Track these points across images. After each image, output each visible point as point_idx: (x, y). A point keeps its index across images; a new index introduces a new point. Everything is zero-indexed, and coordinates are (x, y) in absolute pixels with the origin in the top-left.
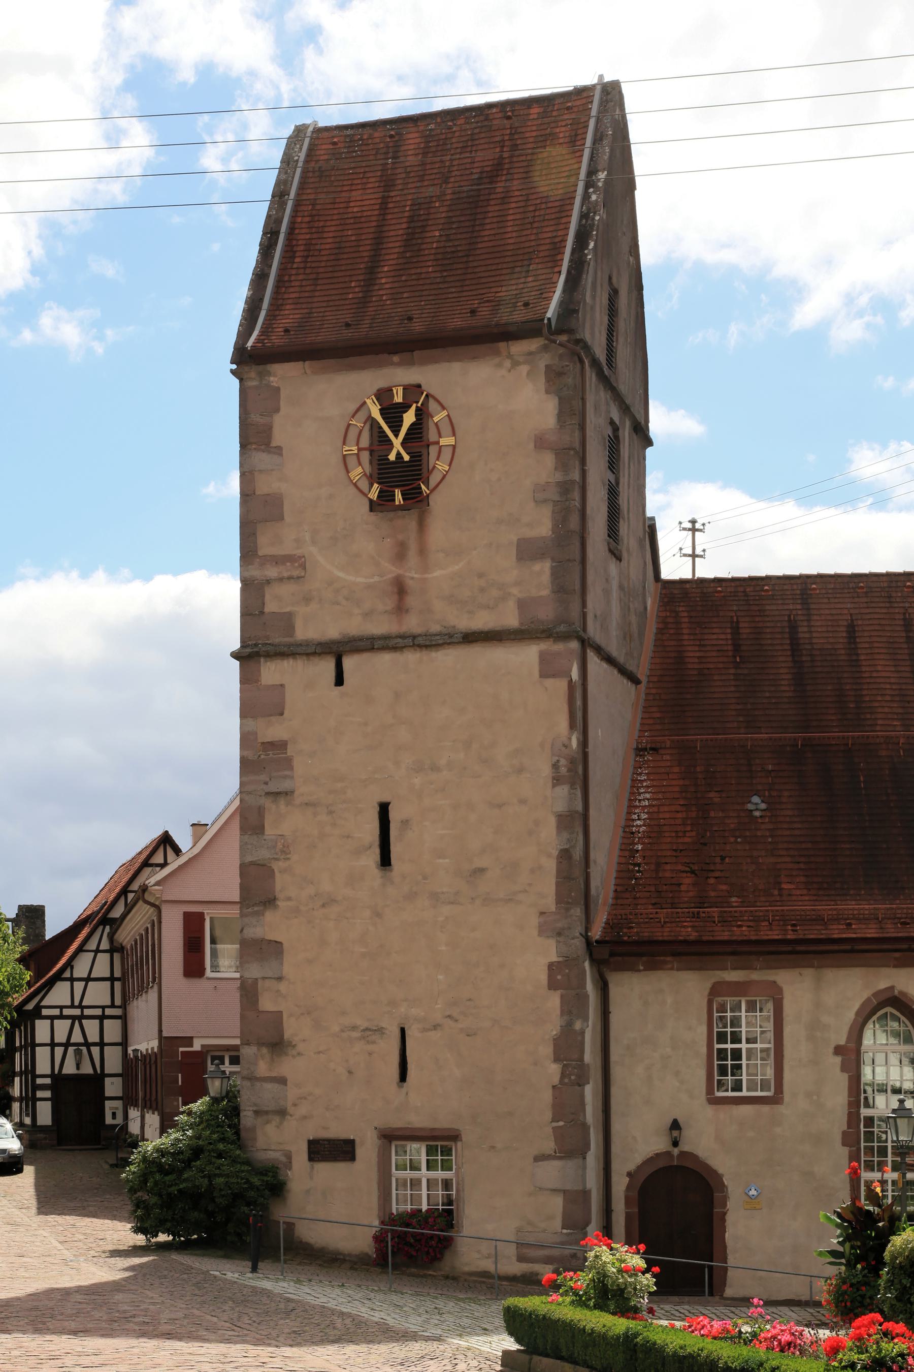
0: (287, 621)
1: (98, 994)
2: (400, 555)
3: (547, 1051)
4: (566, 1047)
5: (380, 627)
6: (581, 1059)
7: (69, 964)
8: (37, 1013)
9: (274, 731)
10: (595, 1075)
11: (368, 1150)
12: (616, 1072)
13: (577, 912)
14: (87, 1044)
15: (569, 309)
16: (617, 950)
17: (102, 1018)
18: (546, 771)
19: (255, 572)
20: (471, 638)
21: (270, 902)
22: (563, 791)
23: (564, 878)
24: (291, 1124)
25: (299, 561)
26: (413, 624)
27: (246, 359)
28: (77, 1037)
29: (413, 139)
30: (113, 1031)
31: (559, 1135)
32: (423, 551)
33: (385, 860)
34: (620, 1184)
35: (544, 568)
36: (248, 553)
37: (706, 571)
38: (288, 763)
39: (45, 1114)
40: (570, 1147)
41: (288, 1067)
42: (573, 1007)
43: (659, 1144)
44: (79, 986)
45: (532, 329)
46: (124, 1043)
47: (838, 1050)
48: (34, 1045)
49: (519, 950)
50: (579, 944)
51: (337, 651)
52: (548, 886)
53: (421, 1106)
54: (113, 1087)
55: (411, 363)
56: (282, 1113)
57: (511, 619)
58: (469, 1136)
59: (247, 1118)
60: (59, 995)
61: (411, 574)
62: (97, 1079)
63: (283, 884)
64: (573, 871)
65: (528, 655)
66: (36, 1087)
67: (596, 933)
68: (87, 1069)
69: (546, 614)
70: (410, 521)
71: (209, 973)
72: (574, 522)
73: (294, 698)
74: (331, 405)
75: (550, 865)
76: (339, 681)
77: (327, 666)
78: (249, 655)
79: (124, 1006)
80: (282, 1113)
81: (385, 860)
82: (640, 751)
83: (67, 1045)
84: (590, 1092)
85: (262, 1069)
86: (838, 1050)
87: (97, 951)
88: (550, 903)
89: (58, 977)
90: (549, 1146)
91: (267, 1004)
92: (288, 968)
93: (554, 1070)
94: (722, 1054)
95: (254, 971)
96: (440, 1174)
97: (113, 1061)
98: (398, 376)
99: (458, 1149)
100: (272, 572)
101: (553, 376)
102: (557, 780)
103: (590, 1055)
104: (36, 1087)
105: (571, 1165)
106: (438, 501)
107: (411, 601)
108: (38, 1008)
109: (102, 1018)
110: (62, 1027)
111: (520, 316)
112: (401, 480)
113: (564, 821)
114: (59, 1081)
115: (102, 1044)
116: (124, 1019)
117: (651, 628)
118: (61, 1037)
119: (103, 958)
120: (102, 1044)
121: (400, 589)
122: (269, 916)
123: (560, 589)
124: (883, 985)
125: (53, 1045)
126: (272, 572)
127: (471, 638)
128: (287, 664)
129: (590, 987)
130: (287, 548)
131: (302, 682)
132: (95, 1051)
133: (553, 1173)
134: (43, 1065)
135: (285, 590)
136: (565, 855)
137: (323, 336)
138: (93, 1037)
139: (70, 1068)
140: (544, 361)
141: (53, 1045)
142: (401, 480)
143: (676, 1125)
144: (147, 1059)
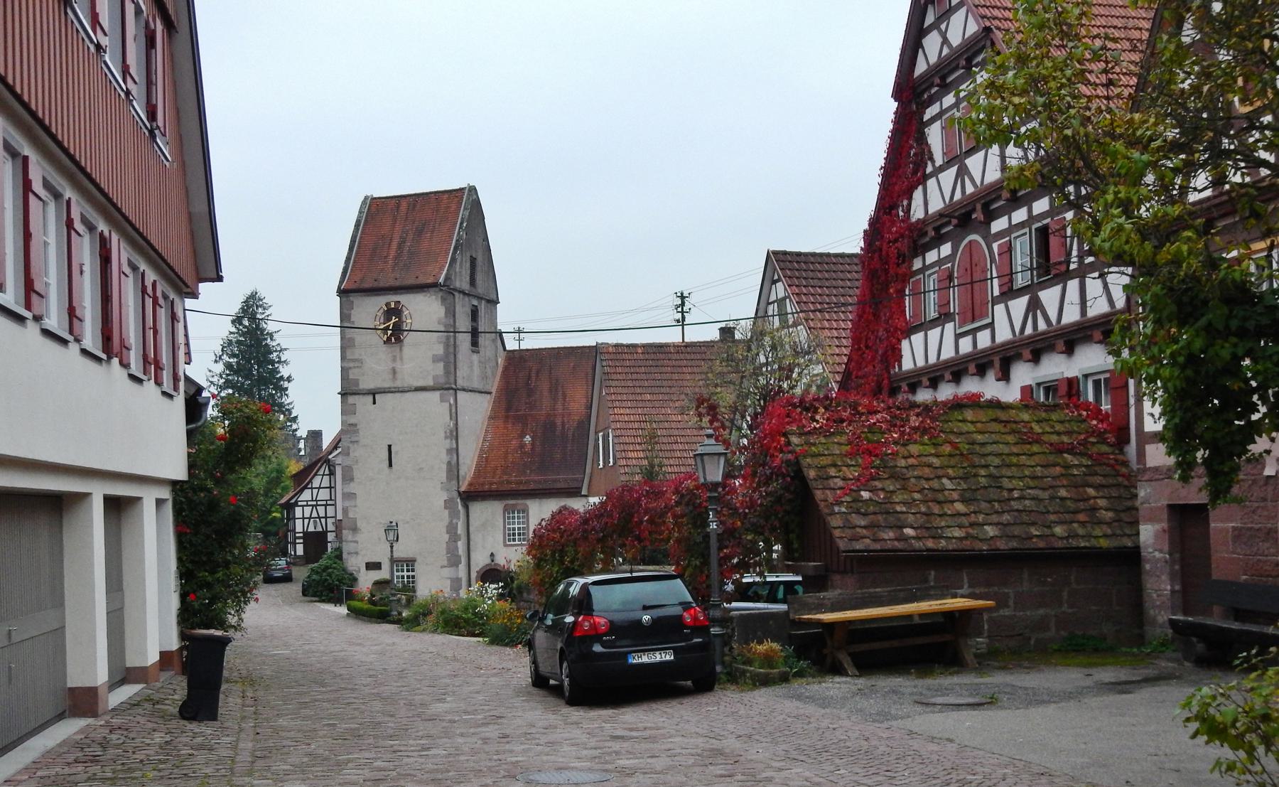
0: (356, 382)
2: (394, 360)
3: (444, 530)
4: (451, 529)
5: (386, 385)
6: (1215, 219)
7: (311, 481)
8: (296, 504)
9: (352, 420)
10: (464, 539)
12: (472, 536)
13: (454, 482)
15: (447, 278)
16: (470, 497)
17: (326, 505)
18: (443, 435)
19: (346, 365)
20: (418, 389)
21: (352, 479)
22: (448, 441)
23: (449, 471)
24: (360, 557)
25: (360, 361)
26: (398, 384)
27: (342, 292)
28: (315, 514)
29: (404, 204)
31: (449, 560)
32: (401, 359)
33: (390, 465)
34: (474, 575)
35: (441, 365)
36: (343, 358)
38: (357, 431)
39: (300, 550)
40: (454, 562)
41: (359, 537)
42: (454, 514)
43: (488, 561)
44: (315, 491)
45: (435, 285)
48: (295, 519)
49: (432, 496)
50: (455, 494)
51: (373, 393)
52: (444, 475)
53: (401, 551)
56: (357, 553)
57: (430, 383)
58: (419, 560)
59: (345, 556)
60: (306, 495)
61: (398, 365)
62: (324, 534)
63: (356, 474)
64: (453, 470)
65: (437, 394)
66: (296, 538)
67: (462, 489)
69: (442, 380)
70: (397, 348)
72: (451, 350)
74: (370, 310)
75: (444, 467)
77: (370, 398)
78: (344, 394)
80: (357, 553)
81: (390, 465)
83: (310, 518)
84: (461, 545)
85: (350, 538)
88: (444, 479)
89: (306, 487)
90: (445, 563)
91: (351, 515)
92: (359, 501)
93: (446, 537)
95: (347, 504)
98: (392, 299)
99: (417, 566)
100: (351, 365)
101: (443, 300)
102: (446, 438)
103: (461, 530)
104: (296, 538)
105: (452, 569)
107: (399, 376)
108: (297, 502)
109: (326, 505)
110: (308, 510)
111: (430, 280)
112: (395, 334)
113: (449, 451)
114: (307, 536)
115: (326, 517)
117: (500, 370)
118: (307, 515)
119: (326, 478)
120: (326, 517)
121: (394, 372)
122: (352, 485)
123: (447, 373)
124: (563, 504)
125: (303, 518)
126: (351, 365)
127: (418, 389)
128: (357, 397)
129: (460, 507)
130: (356, 356)
131: (363, 403)
133: (448, 572)
134: (299, 528)
135: (356, 371)
136: (449, 463)
137: (366, 285)
138: (322, 514)
139: (311, 529)
140: (440, 294)
141: (303, 518)
143: (492, 555)
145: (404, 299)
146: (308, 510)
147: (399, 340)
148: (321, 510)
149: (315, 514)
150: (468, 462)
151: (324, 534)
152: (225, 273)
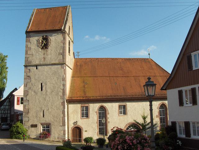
1: (7, 107)
2: (44, 54)
12: (69, 115)
14: (6, 113)
17: (7, 110)
26: (46, 62)
30: (9, 112)
34: (70, 129)
37: (80, 57)
46: (10, 113)
47: (96, 112)
51: (36, 66)
54: (9, 119)
55: (46, 33)
57: (57, 62)
62: (7, 118)
68: (5, 116)
71: (20, 104)
73: (32, 70)
74: (35, 40)
76: (37, 69)
79: (10, 109)
82: (72, 77)
83: (3, 113)
86: (96, 112)
87: (7, 102)
94: (120, 111)
96: (48, 129)
97: (9, 115)
98: (45, 35)
109: (7, 110)
112: (45, 46)
116: (10, 110)
118: (2, 113)
120: (7, 113)
130: (31, 53)
132: (7, 114)
135: (31, 58)
139: (3, 116)
144: (13, 115)
148: (6, 111)
149: (4, 112)
150: (3, 141)
151: (7, 118)
152: (63, 5)
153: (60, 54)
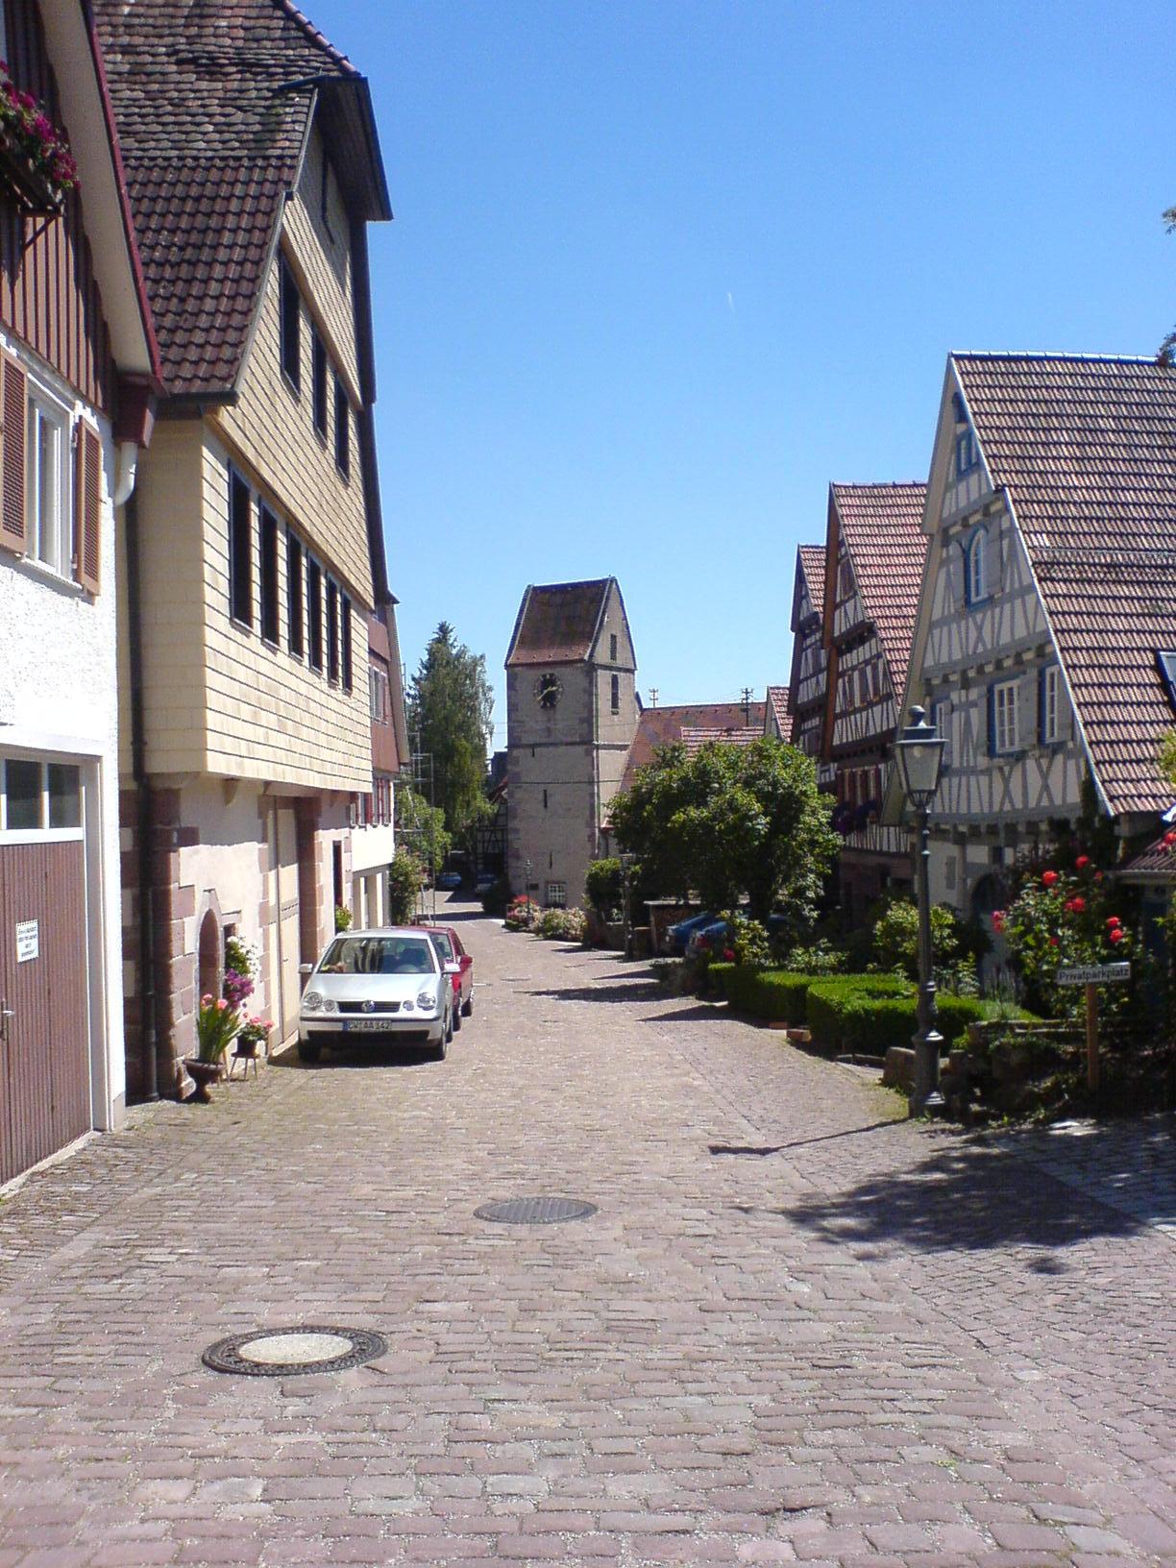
11: (542, 886)
27: (507, 666)
51: (533, 746)
98: (548, 671)
106: (560, 706)
112: (550, 700)
121: (549, 730)
142: (550, 700)
145: (557, 671)
146: (487, 835)
147: (553, 706)
153: (582, 721)
